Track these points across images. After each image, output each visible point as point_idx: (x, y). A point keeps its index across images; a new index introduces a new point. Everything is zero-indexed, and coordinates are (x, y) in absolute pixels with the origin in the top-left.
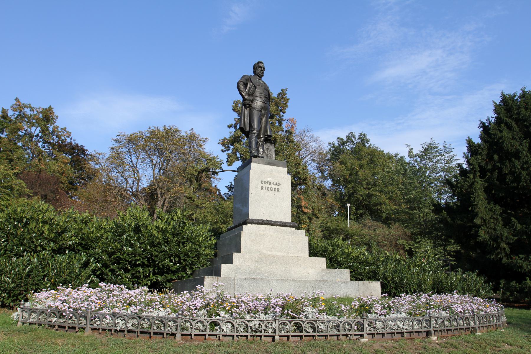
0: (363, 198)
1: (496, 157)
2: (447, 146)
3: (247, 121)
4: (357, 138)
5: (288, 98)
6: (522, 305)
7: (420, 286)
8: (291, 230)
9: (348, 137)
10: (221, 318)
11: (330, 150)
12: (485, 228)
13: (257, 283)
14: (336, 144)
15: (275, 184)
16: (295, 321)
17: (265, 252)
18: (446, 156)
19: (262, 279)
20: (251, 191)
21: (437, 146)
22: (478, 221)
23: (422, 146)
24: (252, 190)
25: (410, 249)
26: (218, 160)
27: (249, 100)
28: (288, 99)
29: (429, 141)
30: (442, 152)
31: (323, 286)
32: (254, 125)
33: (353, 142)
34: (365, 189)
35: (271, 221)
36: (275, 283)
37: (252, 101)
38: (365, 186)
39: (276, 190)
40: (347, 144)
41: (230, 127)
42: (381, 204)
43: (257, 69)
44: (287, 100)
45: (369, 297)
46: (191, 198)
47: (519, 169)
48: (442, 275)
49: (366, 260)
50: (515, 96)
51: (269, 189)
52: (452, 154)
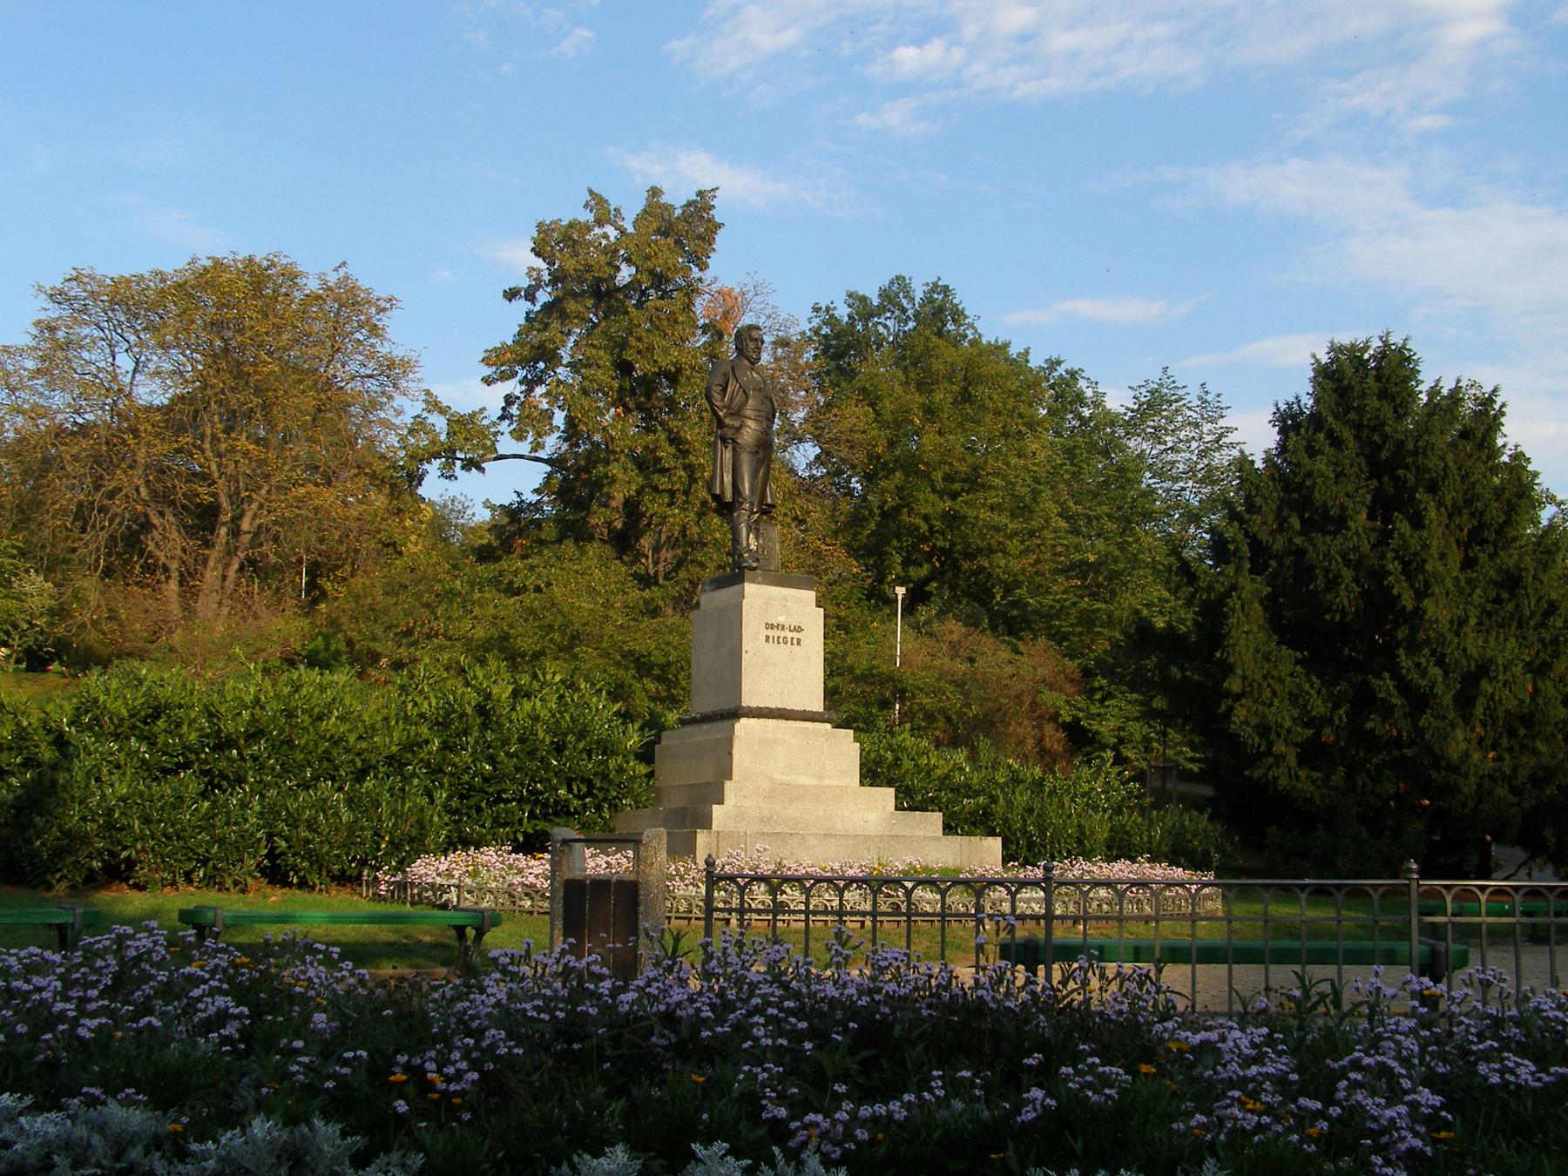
0: (931, 527)
1: (1295, 522)
2: (1209, 398)
3: (728, 479)
4: (917, 300)
5: (718, 220)
6: (1261, 881)
7: (1080, 842)
9: (886, 295)
11: (817, 332)
12: (1250, 704)
14: (843, 312)
16: (891, 900)
17: (777, 776)
18: (1205, 430)
21: (1181, 392)
22: (1234, 685)
23: (1132, 394)
24: (746, 645)
25: (1077, 720)
26: (485, 422)
28: (720, 226)
29: (1155, 375)
30: (1195, 415)
33: (904, 310)
34: (940, 494)
36: (813, 841)
37: (738, 429)
39: (795, 642)
41: (511, 295)
42: (990, 551)
44: (714, 227)
46: (394, 544)
47: (1338, 563)
48: (1131, 819)
50: (1366, 348)
51: (795, 642)
52: (1222, 423)
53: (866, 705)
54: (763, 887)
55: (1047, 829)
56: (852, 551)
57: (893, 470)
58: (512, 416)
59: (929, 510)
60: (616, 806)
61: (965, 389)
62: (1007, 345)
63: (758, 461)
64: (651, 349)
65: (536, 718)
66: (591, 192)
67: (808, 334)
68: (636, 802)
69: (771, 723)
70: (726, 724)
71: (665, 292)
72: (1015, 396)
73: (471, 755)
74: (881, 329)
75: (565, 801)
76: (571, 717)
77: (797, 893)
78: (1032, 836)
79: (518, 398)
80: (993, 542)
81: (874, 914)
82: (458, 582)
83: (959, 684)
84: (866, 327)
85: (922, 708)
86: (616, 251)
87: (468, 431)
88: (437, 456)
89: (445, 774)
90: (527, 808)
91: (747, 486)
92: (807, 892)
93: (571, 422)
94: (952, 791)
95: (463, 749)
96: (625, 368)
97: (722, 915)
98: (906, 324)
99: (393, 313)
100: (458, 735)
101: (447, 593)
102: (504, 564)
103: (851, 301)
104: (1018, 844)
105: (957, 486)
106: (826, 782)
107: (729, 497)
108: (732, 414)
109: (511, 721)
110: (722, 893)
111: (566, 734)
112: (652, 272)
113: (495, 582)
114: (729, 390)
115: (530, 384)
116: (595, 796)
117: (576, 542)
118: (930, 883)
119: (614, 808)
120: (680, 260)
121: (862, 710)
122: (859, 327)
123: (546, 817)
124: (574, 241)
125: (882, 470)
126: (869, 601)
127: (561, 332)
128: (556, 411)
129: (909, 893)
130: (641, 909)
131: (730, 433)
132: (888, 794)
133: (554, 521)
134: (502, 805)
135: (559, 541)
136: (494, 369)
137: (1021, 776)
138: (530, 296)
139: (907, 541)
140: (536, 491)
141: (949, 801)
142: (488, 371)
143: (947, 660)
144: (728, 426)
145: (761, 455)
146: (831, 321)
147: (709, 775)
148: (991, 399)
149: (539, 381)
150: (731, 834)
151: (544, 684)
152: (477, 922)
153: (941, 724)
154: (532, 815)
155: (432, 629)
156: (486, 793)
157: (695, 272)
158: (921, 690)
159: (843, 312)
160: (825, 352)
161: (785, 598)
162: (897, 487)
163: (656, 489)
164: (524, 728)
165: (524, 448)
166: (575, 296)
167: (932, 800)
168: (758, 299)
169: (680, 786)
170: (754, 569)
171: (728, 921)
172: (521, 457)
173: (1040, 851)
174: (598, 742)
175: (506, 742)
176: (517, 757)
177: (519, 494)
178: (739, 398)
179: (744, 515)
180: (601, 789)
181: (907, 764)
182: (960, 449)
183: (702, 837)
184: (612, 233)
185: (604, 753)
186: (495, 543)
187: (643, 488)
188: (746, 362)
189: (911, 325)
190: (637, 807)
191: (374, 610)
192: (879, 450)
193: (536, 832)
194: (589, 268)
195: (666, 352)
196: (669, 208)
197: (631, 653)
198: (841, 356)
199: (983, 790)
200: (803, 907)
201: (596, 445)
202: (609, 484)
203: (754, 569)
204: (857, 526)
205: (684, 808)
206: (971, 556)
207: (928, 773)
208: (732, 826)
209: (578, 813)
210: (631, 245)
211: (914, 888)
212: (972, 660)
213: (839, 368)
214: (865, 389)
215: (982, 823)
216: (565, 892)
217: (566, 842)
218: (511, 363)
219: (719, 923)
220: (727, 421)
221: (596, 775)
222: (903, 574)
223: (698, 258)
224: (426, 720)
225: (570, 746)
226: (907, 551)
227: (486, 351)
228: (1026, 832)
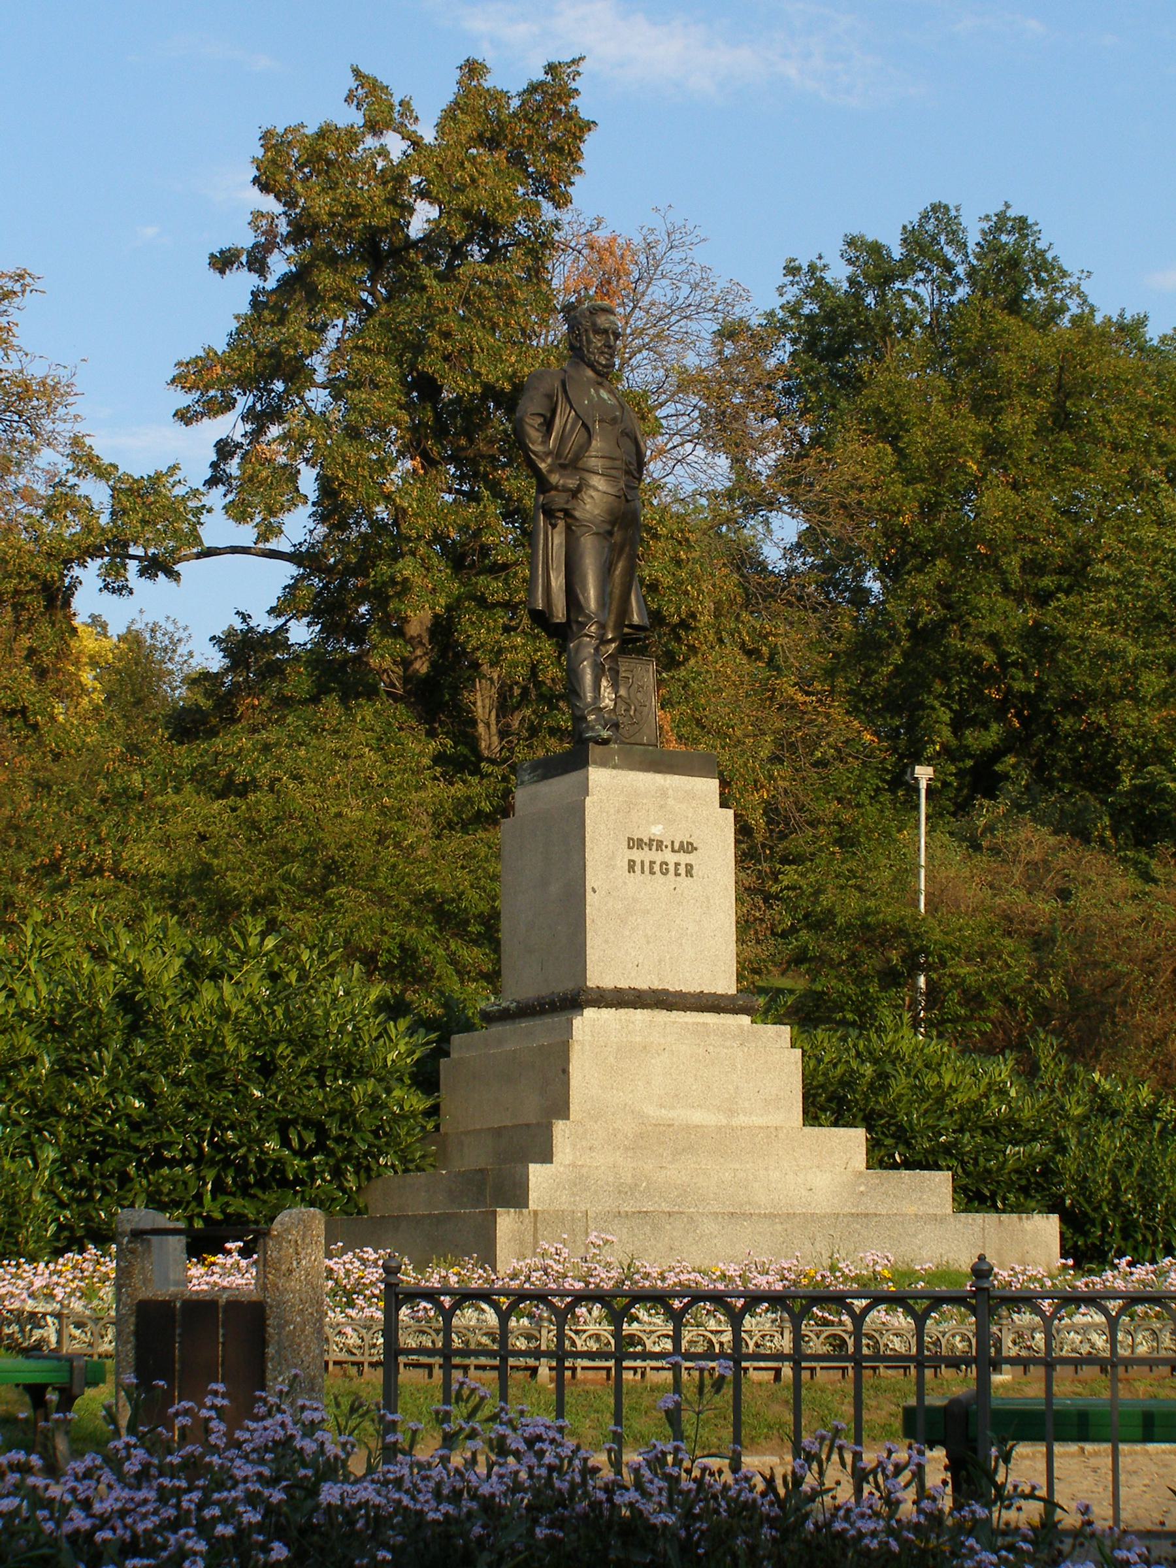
0: (1002, 657)
3: (558, 582)
4: (972, 247)
5: (585, 114)
8: (740, 1027)
9: (914, 239)
10: (648, 1328)
11: (794, 311)
13: (655, 1228)
14: (839, 273)
15: (677, 846)
16: (829, 1330)
17: (651, 1111)
19: (670, 1214)
20: (591, 880)
24: (594, 877)
26: (180, 491)
27: (565, 489)
28: (588, 126)
31: (864, 1233)
32: (587, 599)
33: (948, 267)
34: (1018, 597)
35: (665, 992)
36: (709, 1226)
37: (575, 493)
38: (1016, 579)
39: (682, 870)
40: (909, 285)
41: (223, 262)
43: (589, 342)
45: (1018, 1269)
49: (1012, 1119)
51: (657, 868)
53: (860, 980)
54: (597, 1309)
55: (1157, 1199)
56: (859, 704)
57: (934, 554)
58: (230, 476)
59: (997, 626)
60: (368, 1169)
61: (1060, 405)
62: (1141, 322)
63: (612, 548)
64: (468, 352)
65: (224, 1016)
66: (357, 73)
67: (781, 314)
68: (404, 1160)
69: (639, 1016)
70: (556, 1020)
71: (495, 249)
72: (1151, 415)
73: (107, 1083)
74: (908, 301)
75: (278, 1160)
76: (287, 1011)
77: (658, 1320)
78: (1130, 1211)
79: (239, 446)
80: (1114, 680)
81: (797, 1358)
82: (136, 777)
83: (1040, 942)
84: (881, 299)
85: (959, 983)
86: (401, 179)
87: (148, 507)
88: (95, 552)
89: (59, 1115)
90: (210, 1175)
91: (592, 593)
92: (676, 1318)
93: (327, 487)
94: (985, 1131)
95: (93, 1072)
96: (428, 387)
97: (522, 1362)
98: (953, 291)
99: (28, 299)
100: (84, 1048)
101: (118, 795)
102: (218, 743)
103: (852, 253)
104: (1105, 1226)
105: (1047, 582)
106: (741, 1120)
107: (560, 614)
108: (563, 467)
109: (180, 1022)
110: (525, 1321)
111: (276, 1043)
112: (466, 214)
113: (200, 777)
114: (558, 423)
115: (259, 419)
116: (330, 1153)
117: (344, 700)
118: (658, 1299)
119: (365, 1171)
120: (521, 191)
121: (851, 989)
122: (870, 299)
123: (244, 1190)
124: (329, 163)
125: (913, 555)
126: (894, 792)
127: (310, 327)
128: (302, 466)
129: (859, 1319)
130: (271, 1351)
131: (559, 500)
132: (855, 1138)
133: (308, 663)
134: (165, 1171)
135: (315, 700)
136: (196, 395)
137: (1114, 1103)
138: (258, 264)
139: (960, 684)
140: (272, 611)
141: (978, 1150)
142: (185, 399)
143: (1021, 895)
144: (556, 488)
145: (618, 537)
146: (819, 289)
147: (530, 1115)
148: (1107, 421)
149: (275, 414)
150: (560, 1217)
151: (244, 956)
152: (60, 1378)
153: (993, 1013)
154: (219, 1188)
155: (91, 859)
156: (136, 1149)
157: (548, 211)
158: (957, 951)
159: (839, 273)
160: (810, 346)
161: (664, 793)
162: (938, 586)
163: (482, 602)
164: (204, 1034)
165: (246, 535)
166: (332, 260)
167: (947, 1150)
168: (676, 255)
169: (481, 1131)
170: (605, 742)
171: (534, 1371)
172: (244, 550)
173: (1145, 1240)
174: (335, 1056)
175: (170, 1059)
176: (191, 1085)
177: (245, 617)
178: (576, 438)
179: (588, 646)
180: (339, 1139)
181: (900, 1085)
182: (1050, 514)
183: (506, 1222)
184: (396, 146)
185: (346, 1075)
186: (205, 704)
187: (459, 600)
188: (590, 373)
189: (962, 291)
190: (406, 1171)
191: (17, 828)
192: (905, 520)
193: (228, 1216)
194: (354, 211)
195: (496, 357)
196: (498, 97)
197: (429, 895)
198: (835, 353)
199: (1041, 1130)
200: (668, 1345)
201: (379, 527)
202: (400, 595)
203: (605, 742)
204: (870, 658)
205: (481, 1170)
206: (1074, 707)
207: (940, 1101)
208: (564, 1201)
209: (302, 1183)
210: (429, 167)
211: (867, 1310)
212: (1064, 894)
213: (833, 373)
214: (877, 411)
215: (1040, 1188)
216: (137, 1325)
217: (138, 1234)
218: (224, 385)
219: (519, 1375)
220: (554, 479)
221: (331, 1114)
222: (954, 743)
223: (553, 186)
224: (30, 1022)
225: (284, 1064)
226: (961, 702)
227: (179, 364)
228: (1119, 1204)
